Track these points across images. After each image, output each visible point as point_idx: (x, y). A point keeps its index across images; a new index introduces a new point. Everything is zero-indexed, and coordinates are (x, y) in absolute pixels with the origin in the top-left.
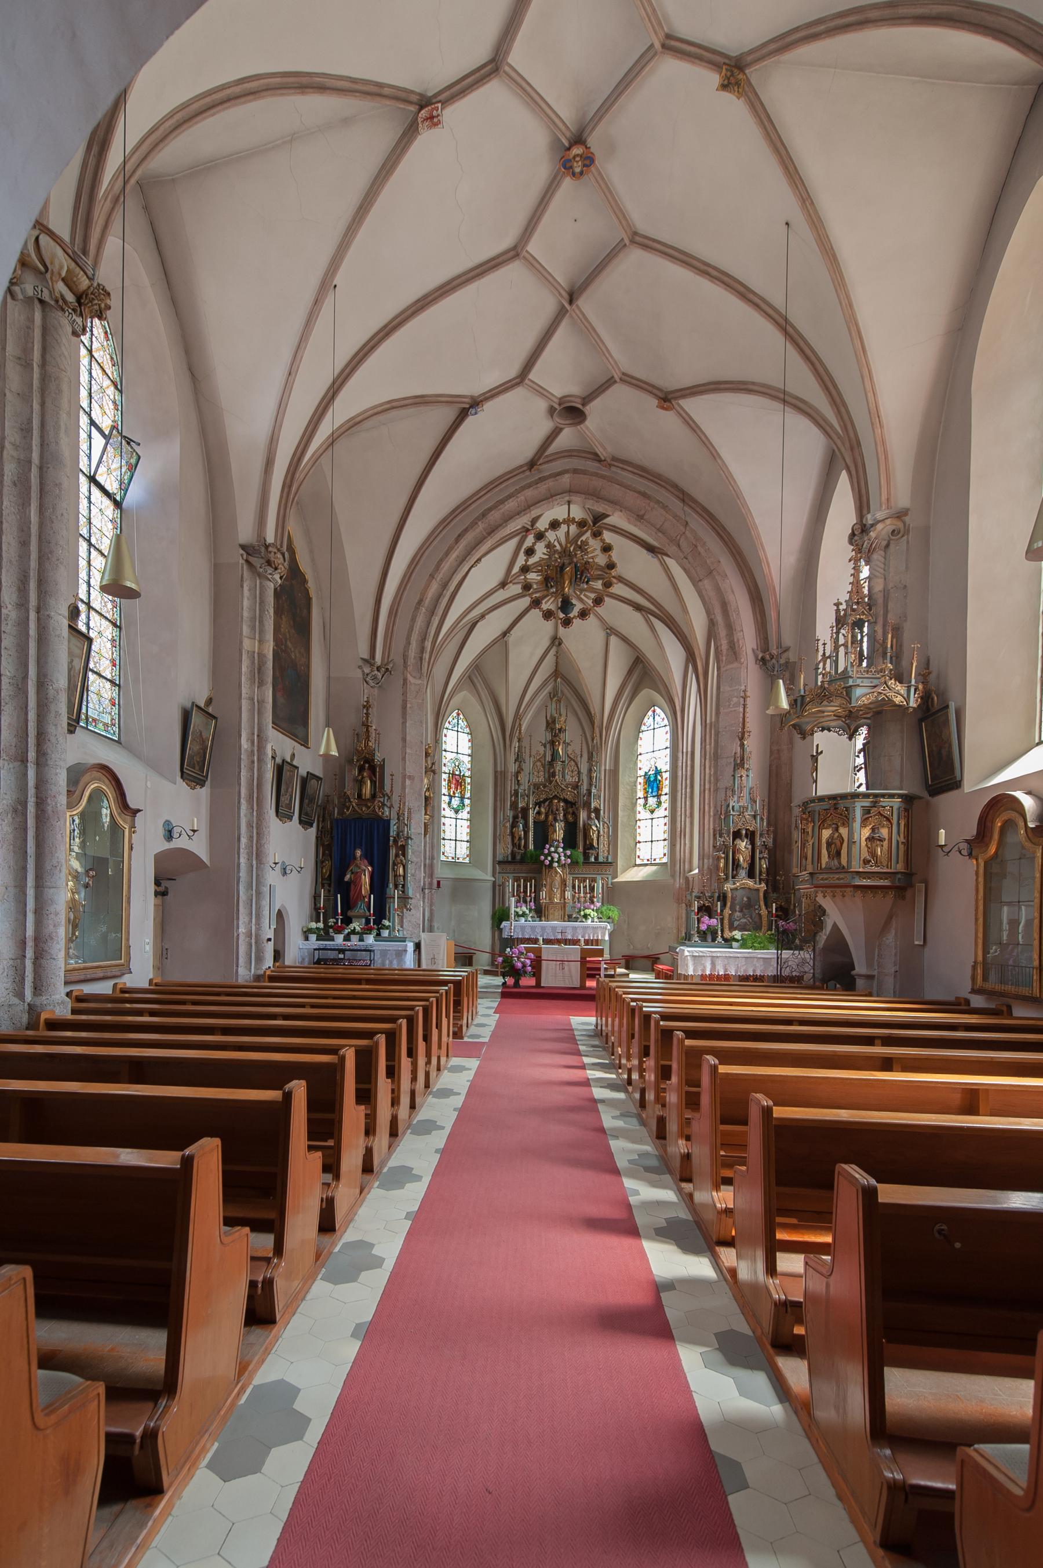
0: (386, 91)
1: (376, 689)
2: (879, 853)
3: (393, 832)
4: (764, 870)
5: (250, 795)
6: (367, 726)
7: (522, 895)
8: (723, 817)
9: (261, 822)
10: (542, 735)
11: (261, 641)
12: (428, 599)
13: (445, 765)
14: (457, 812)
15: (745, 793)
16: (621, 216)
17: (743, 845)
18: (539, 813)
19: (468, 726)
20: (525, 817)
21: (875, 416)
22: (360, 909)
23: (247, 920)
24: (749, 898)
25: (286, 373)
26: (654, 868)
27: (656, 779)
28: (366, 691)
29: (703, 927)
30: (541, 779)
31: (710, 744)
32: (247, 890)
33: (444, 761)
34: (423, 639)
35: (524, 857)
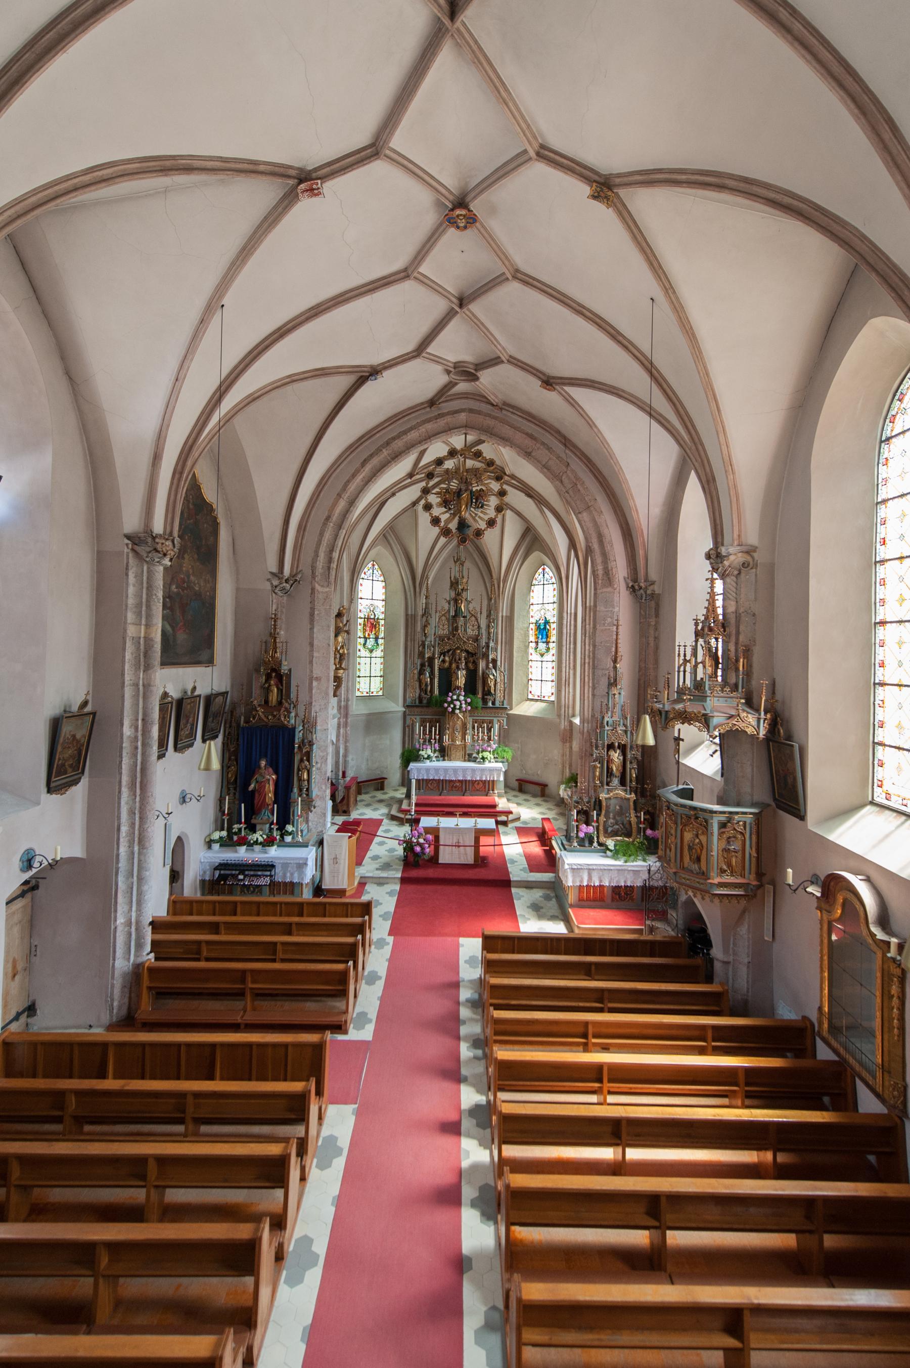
0: (262, 168)
1: (285, 598)
2: (734, 864)
3: (299, 736)
4: (634, 779)
5: (132, 781)
6: (274, 636)
7: (427, 737)
8: (598, 731)
9: (145, 806)
10: (449, 594)
11: (148, 626)
12: (336, 515)
13: (360, 611)
14: (371, 651)
15: (618, 709)
16: (502, 257)
17: (616, 756)
18: (444, 661)
19: (383, 575)
20: (431, 666)
21: (728, 463)
22: (265, 815)
23: (126, 908)
24: (620, 807)
25: (173, 379)
26: (543, 705)
27: (545, 628)
28: (274, 601)
29: (581, 835)
30: (446, 632)
31: (589, 625)
32: (127, 878)
33: (360, 607)
34: (331, 551)
35: (430, 701)
